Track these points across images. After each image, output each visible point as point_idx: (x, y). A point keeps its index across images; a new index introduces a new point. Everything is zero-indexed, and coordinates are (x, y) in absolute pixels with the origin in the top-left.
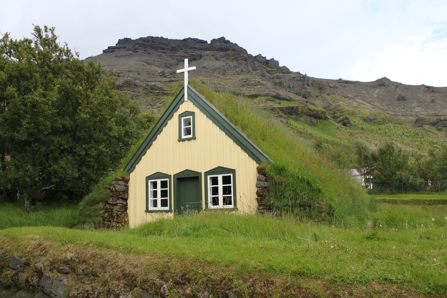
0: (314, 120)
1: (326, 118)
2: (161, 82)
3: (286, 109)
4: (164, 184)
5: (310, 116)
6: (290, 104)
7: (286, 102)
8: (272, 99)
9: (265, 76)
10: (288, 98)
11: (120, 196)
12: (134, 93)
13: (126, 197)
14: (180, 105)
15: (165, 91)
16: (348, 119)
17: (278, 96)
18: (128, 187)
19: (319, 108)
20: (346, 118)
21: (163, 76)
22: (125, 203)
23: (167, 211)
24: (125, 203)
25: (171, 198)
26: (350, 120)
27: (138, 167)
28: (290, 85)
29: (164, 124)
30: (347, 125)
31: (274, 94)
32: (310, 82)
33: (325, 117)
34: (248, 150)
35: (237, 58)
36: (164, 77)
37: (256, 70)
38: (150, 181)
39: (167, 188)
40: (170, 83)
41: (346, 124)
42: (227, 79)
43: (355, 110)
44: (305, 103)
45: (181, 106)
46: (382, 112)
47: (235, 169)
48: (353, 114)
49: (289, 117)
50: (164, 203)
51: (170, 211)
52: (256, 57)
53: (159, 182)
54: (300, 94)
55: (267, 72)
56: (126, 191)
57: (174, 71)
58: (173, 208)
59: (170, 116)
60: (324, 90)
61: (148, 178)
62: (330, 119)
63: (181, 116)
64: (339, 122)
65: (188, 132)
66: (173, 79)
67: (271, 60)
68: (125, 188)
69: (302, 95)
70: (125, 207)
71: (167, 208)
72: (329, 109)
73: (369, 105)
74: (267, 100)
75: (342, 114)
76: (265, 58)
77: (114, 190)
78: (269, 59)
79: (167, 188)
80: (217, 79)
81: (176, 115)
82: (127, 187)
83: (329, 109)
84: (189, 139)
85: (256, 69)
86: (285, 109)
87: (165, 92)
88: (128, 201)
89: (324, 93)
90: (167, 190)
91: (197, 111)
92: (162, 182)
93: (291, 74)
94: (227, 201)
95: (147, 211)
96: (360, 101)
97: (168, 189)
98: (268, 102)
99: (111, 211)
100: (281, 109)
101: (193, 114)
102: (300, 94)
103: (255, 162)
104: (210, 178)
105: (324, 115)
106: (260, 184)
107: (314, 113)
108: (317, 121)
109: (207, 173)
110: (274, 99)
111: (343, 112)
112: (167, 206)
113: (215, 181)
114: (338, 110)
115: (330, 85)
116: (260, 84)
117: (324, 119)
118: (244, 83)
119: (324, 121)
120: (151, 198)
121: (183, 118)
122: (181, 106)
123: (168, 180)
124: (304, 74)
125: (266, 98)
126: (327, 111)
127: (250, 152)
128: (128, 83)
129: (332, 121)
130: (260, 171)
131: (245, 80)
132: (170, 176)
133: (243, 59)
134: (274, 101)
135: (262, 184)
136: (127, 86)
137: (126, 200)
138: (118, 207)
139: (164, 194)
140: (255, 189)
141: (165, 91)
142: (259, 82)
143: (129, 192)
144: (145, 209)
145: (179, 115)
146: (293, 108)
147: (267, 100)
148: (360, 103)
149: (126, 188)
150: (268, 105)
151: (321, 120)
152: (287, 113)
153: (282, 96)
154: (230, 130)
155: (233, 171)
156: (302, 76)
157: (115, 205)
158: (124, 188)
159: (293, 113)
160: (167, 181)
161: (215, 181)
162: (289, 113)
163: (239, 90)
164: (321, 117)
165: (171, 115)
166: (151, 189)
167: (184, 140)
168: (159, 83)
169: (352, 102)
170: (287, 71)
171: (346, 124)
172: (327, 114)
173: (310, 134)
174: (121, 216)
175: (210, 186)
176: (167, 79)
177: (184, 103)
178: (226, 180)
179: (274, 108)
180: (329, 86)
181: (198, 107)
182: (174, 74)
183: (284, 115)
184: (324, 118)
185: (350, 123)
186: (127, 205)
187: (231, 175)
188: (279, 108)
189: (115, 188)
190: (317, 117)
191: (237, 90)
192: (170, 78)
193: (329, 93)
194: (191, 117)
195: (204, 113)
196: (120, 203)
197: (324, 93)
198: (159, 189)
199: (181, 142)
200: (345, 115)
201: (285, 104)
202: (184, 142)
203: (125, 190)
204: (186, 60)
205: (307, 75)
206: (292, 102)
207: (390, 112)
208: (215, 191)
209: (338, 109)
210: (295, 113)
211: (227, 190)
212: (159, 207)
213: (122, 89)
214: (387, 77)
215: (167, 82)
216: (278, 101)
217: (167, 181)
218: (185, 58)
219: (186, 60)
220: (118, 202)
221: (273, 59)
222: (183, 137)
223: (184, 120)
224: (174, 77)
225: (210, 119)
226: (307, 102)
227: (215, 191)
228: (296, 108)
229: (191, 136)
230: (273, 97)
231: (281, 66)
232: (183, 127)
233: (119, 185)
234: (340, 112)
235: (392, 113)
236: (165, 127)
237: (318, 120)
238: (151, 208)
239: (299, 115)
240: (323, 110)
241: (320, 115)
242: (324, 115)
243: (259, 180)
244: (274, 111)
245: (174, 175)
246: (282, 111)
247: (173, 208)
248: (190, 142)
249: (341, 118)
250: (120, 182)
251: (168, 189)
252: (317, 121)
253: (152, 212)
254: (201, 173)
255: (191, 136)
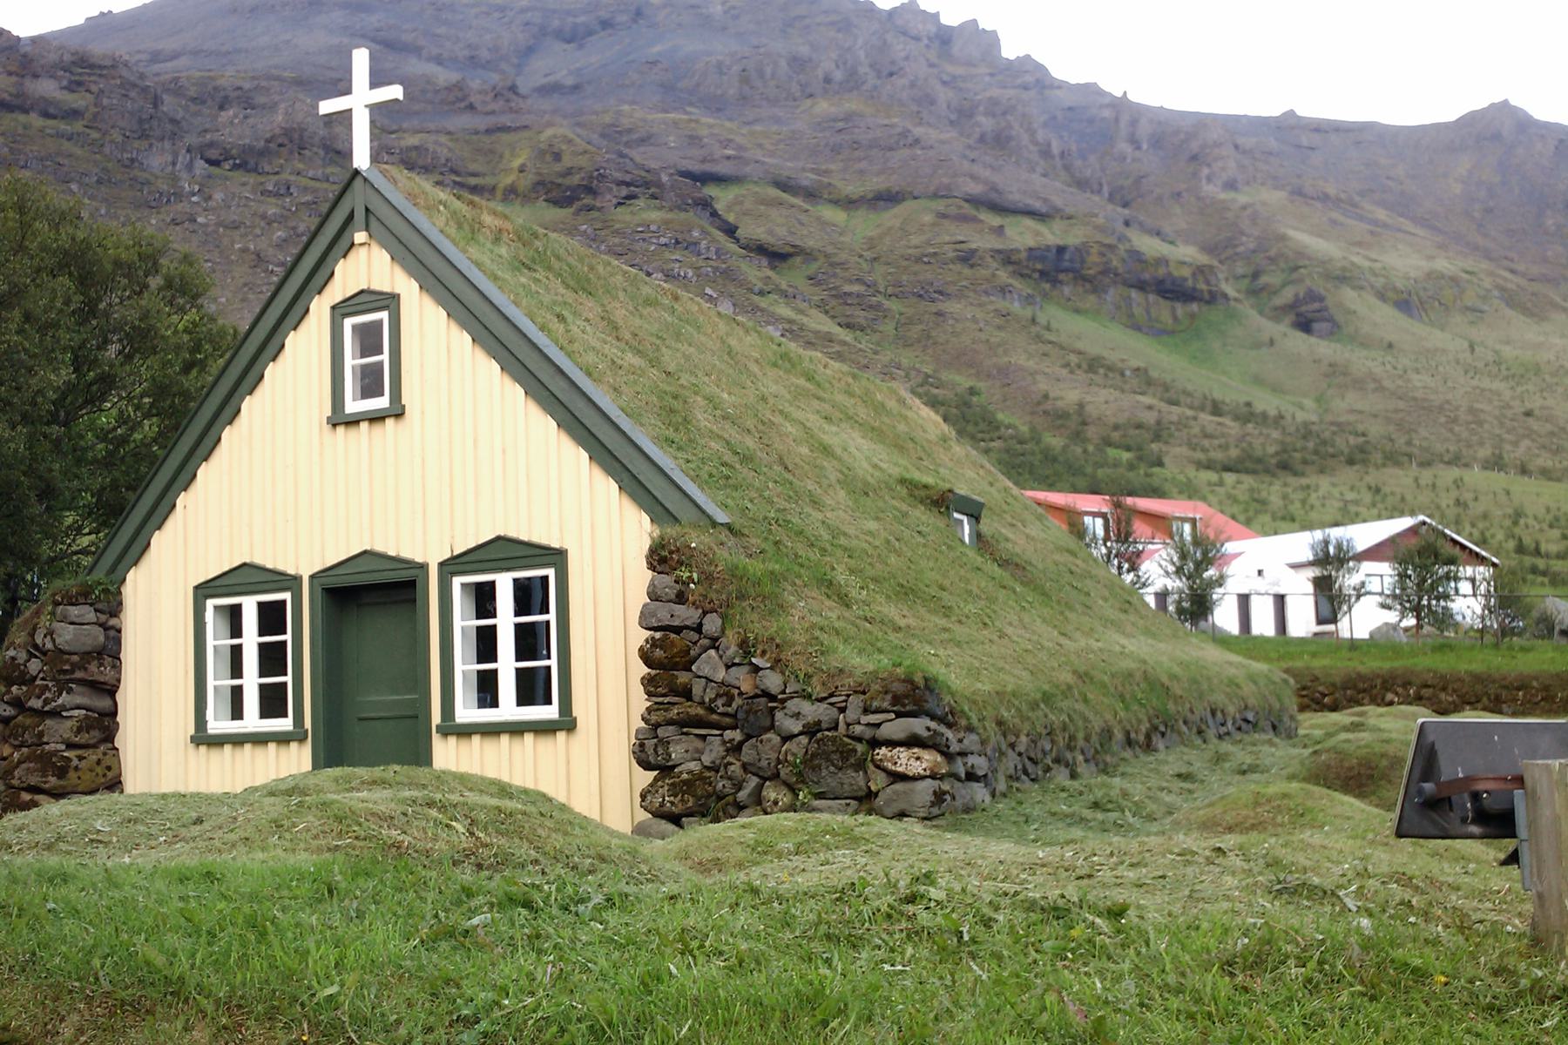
0: (1163, 311)
1: (1213, 298)
2: (449, 133)
3: (1029, 258)
4: (271, 618)
5: (1141, 286)
6: (1051, 235)
7: (1028, 222)
8: (968, 209)
9: (932, 102)
10: (1038, 205)
11: (79, 675)
12: (325, 185)
13: (107, 674)
14: (337, 262)
15: (474, 175)
16: (1321, 299)
17: (994, 196)
18: (119, 631)
19: (1184, 254)
20: (1312, 296)
21: (463, 105)
22: (103, 703)
23: (282, 739)
24: (103, 703)
25: (302, 678)
26: (1329, 302)
27: (162, 541)
28: (1049, 145)
29: (270, 347)
30: (1316, 326)
31: (975, 189)
32: (1144, 130)
33: (1210, 292)
34: (617, 465)
35: (804, 17)
36: (466, 107)
37: (891, 74)
38: (211, 603)
39: (284, 632)
40: (493, 138)
41: (1311, 321)
42: (756, 121)
43: (1355, 259)
44: (1120, 227)
45: (339, 269)
46: (1485, 265)
47: (565, 547)
48: (1344, 278)
49: (1045, 295)
50: (272, 702)
51: (296, 736)
52: (892, 13)
53: (249, 608)
54: (1095, 187)
55: (944, 83)
56: (110, 650)
57: (509, 83)
58: (308, 724)
59: (294, 314)
60: (1209, 165)
61: (204, 591)
62: (1236, 300)
63: (341, 310)
64: (1278, 313)
65: (370, 383)
66: (506, 120)
67: (963, 26)
68: (102, 638)
69: (1106, 189)
70: (104, 725)
71: (284, 724)
72: (1230, 252)
73: (1421, 232)
74: (944, 216)
75: (1295, 276)
76: (936, 16)
77: (49, 646)
78: (955, 24)
79: (284, 632)
80: (711, 121)
81: (320, 308)
82: (112, 633)
83: (1230, 252)
84: (376, 418)
85: (895, 69)
86: (1024, 255)
87: (473, 181)
88: (119, 697)
89: (1209, 179)
90: (284, 643)
91: (407, 288)
92: (262, 607)
93: (1058, 92)
94: (531, 688)
95: (203, 738)
96: (1381, 214)
97: (288, 637)
98: (946, 222)
99: (35, 740)
100: (1007, 258)
101: (390, 301)
102: (1095, 187)
103: (646, 519)
104: (463, 585)
105: (1208, 283)
106: (653, 615)
107: (1162, 271)
108: (1173, 311)
109: (453, 565)
110: (973, 212)
111: (1296, 268)
112: (285, 715)
113: (484, 599)
114: (1272, 260)
115: (1241, 141)
116: (910, 140)
117: (1208, 302)
118: (838, 138)
119: (1205, 308)
120: (218, 681)
121: (349, 323)
122: (340, 268)
123: (286, 596)
124: (1119, 94)
125: (940, 205)
126: (1221, 262)
127: (625, 475)
128: (296, 136)
129: (1248, 310)
130: (660, 558)
131: (841, 125)
132: (297, 579)
133: (832, 24)
134: (974, 219)
135: (664, 614)
136: (291, 152)
137: (111, 690)
138: (69, 723)
139: (272, 659)
140: (640, 636)
141: (474, 175)
142: (905, 134)
143: (122, 656)
144: (192, 731)
145: (333, 308)
146: (1061, 250)
147: (944, 216)
148: (1376, 222)
149: (107, 637)
150: (947, 238)
151: (1194, 307)
152: (1036, 275)
153: (1010, 197)
154: (546, 375)
155: (557, 557)
156: (1107, 101)
157: (56, 714)
158: (100, 636)
159: (1062, 276)
160: (284, 602)
161: (484, 599)
162: (1042, 273)
163: (812, 170)
164: (1194, 289)
165: (298, 309)
166: (216, 640)
167: (353, 422)
168: (443, 139)
169: (1341, 219)
170: (1038, 81)
171: (1311, 321)
172: (1221, 276)
173: (1138, 369)
174: (83, 764)
175: (464, 622)
176: (481, 123)
177: (352, 255)
178: (528, 597)
179: (974, 252)
180: (1236, 147)
181: (411, 273)
182: (511, 95)
183: (1019, 286)
184: (1207, 296)
185: (1331, 320)
186: (114, 713)
187: (550, 573)
188: (999, 252)
189: (53, 641)
190: (1172, 291)
191: (804, 170)
192: (493, 113)
193: (1235, 181)
194: (384, 316)
195: (440, 302)
196: (78, 707)
197: (1209, 179)
198: (251, 640)
199: (341, 430)
200: (1308, 282)
201: (1023, 235)
202: (353, 433)
203: (104, 647)
204: (361, 60)
205: (1131, 97)
206: (1058, 225)
207: (1521, 267)
208: (486, 644)
209: (1272, 253)
210: (1071, 275)
211: (529, 641)
212: (252, 720)
213: (267, 168)
214: (1513, 102)
215: (477, 133)
216: (995, 220)
217: (284, 602)
218: (358, 46)
219: (361, 60)
220: (64, 699)
221: (975, 21)
222: (353, 406)
223: (355, 328)
224: (511, 110)
225: (464, 326)
226: (1127, 224)
227: (486, 644)
228: (1077, 249)
229: (382, 402)
230: (974, 201)
231: (1012, 57)
232: (351, 362)
233: (72, 623)
234: (1282, 265)
235: (1535, 270)
236: (274, 359)
237: (1180, 309)
238: (218, 724)
239: (1088, 286)
240: (1204, 259)
241: (1190, 283)
242: (1208, 283)
243: (654, 595)
244: (972, 266)
245: (312, 577)
246: (1011, 268)
247: (308, 724)
248: (377, 429)
249: (1287, 295)
250: (74, 611)
251: (288, 637)
252: (1173, 311)
253: (218, 741)
254: (423, 567)
255: (382, 402)
